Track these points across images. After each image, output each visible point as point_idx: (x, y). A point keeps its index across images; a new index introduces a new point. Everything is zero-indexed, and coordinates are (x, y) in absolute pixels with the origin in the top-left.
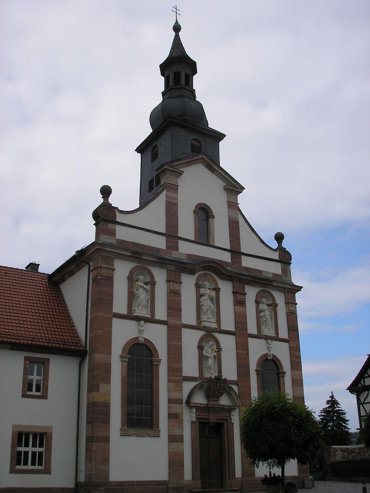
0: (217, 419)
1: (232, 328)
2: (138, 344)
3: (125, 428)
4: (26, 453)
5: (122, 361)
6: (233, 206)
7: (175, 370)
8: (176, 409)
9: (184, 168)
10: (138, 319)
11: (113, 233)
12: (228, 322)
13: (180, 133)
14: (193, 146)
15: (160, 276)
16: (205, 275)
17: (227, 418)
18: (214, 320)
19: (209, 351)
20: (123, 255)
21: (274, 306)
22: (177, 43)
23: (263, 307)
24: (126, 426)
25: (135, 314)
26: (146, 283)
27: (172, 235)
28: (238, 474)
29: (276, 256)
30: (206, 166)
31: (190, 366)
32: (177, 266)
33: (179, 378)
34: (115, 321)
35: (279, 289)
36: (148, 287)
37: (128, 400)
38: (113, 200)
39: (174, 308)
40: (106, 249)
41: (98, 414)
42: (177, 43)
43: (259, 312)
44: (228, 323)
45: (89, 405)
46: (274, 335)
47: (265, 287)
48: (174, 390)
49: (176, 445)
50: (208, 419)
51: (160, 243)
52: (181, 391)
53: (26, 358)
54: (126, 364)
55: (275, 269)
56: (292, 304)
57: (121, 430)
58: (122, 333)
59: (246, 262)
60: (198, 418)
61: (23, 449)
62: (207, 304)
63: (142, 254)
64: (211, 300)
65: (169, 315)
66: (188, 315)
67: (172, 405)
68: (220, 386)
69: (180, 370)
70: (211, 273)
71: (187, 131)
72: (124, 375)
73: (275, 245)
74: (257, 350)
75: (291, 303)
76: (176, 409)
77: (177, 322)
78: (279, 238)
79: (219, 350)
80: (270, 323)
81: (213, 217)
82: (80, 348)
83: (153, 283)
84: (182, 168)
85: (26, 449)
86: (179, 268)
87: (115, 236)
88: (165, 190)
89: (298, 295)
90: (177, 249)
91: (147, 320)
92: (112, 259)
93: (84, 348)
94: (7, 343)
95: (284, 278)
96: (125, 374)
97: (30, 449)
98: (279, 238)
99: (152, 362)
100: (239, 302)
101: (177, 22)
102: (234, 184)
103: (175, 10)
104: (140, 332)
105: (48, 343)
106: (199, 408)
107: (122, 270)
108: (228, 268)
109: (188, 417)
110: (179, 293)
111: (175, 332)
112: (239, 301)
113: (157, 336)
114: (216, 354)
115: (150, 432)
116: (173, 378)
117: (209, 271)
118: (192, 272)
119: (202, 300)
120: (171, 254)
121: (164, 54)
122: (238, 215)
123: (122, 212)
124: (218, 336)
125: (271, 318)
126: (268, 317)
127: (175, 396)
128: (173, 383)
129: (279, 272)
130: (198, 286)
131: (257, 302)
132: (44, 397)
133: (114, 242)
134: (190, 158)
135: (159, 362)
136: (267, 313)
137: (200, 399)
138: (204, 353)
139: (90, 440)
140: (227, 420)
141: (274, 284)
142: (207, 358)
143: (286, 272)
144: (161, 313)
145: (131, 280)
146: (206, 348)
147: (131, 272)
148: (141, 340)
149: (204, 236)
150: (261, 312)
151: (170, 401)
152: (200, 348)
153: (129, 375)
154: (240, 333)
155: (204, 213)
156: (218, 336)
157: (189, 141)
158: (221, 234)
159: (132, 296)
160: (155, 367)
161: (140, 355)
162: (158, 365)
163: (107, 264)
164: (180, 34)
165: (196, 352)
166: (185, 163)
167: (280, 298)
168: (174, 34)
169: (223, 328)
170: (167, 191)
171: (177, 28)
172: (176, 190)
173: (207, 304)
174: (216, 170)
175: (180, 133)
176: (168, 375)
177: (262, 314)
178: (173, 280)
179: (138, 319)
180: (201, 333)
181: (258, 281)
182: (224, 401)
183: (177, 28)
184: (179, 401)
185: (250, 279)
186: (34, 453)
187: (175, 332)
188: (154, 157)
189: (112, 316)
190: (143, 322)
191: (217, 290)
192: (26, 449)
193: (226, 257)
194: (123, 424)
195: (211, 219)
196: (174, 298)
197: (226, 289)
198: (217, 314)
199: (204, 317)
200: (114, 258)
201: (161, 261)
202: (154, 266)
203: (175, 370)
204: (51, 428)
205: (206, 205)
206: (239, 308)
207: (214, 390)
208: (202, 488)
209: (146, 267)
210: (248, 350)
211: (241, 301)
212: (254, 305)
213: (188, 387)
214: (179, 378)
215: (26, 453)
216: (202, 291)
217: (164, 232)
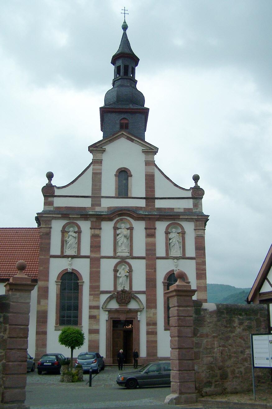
0: (126, 318)
2: (68, 273)
3: (58, 326)
5: (57, 285)
6: (150, 163)
7: (95, 290)
8: (95, 312)
9: (106, 146)
10: (68, 257)
12: (140, 249)
13: (125, 113)
16: (121, 220)
17: (135, 317)
20: (56, 217)
22: (125, 41)
24: (59, 324)
25: (66, 254)
27: (96, 197)
28: (143, 353)
30: (127, 139)
32: (96, 217)
33: (97, 292)
34: (52, 260)
38: (54, 182)
39: (96, 246)
40: (44, 216)
42: (125, 41)
43: (168, 239)
47: (174, 220)
48: (93, 300)
49: (93, 335)
50: (120, 318)
51: (87, 203)
52: (99, 301)
54: (60, 286)
55: (189, 204)
56: (200, 230)
57: (55, 327)
58: (57, 267)
59: (159, 204)
60: (111, 318)
63: (69, 215)
64: (125, 236)
65: (91, 251)
66: (107, 248)
67: (91, 310)
68: (125, 296)
69: (98, 287)
70: (129, 218)
71: (117, 114)
72: (58, 293)
74: (163, 269)
76: (95, 312)
79: (131, 271)
81: (131, 176)
83: (79, 232)
84: (104, 146)
86: (97, 219)
88: (92, 165)
90: (99, 205)
92: (50, 221)
96: (59, 293)
101: (125, 22)
102: (150, 146)
103: (123, 12)
104: (71, 265)
105: (35, 277)
106: (110, 311)
109: (104, 317)
110: (99, 236)
111: (95, 263)
112: (151, 234)
113: (82, 267)
114: (127, 274)
117: (125, 216)
118: (110, 219)
119: (118, 237)
120: (95, 209)
122: (154, 169)
123: (59, 188)
127: (94, 304)
128: (93, 296)
129: (191, 206)
134: (111, 137)
135: (83, 283)
137: (114, 305)
138: (118, 275)
140: (135, 318)
141: (181, 217)
144: (86, 250)
145: (64, 232)
147: (64, 227)
149: (123, 191)
151: (91, 307)
152: (116, 271)
155: (123, 174)
157: (118, 122)
158: (138, 187)
159: (63, 242)
161: (70, 280)
162: (82, 285)
165: (112, 274)
166: (108, 141)
168: (122, 31)
169: (135, 255)
170: (93, 165)
171: (125, 27)
173: (121, 240)
178: (96, 227)
179: (68, 257)
180: (116, 261)
181: (166, 217)
182: (133, 305)
183: (125, 27)
184: (97, 307)
185: (158, 217)
187: (95, 263)
189: (49, 257)
190: (70, 258)
191: (131, 229)
193: (142, 203)
194: (56, 324)
195: (129, 178)
198: (130, 246)
199: (119, 250)
200: (51, 220)
203: (95, 290)
205: (126, 168)
206: (150, 240)
207: (121, 299)
208: (113, 363)
209: (74, 222)
210: (155, 269)
211: (150, 234)
212: (164, 235)
213: (104, 297)
214: (97, 292)
216: (118, 232)
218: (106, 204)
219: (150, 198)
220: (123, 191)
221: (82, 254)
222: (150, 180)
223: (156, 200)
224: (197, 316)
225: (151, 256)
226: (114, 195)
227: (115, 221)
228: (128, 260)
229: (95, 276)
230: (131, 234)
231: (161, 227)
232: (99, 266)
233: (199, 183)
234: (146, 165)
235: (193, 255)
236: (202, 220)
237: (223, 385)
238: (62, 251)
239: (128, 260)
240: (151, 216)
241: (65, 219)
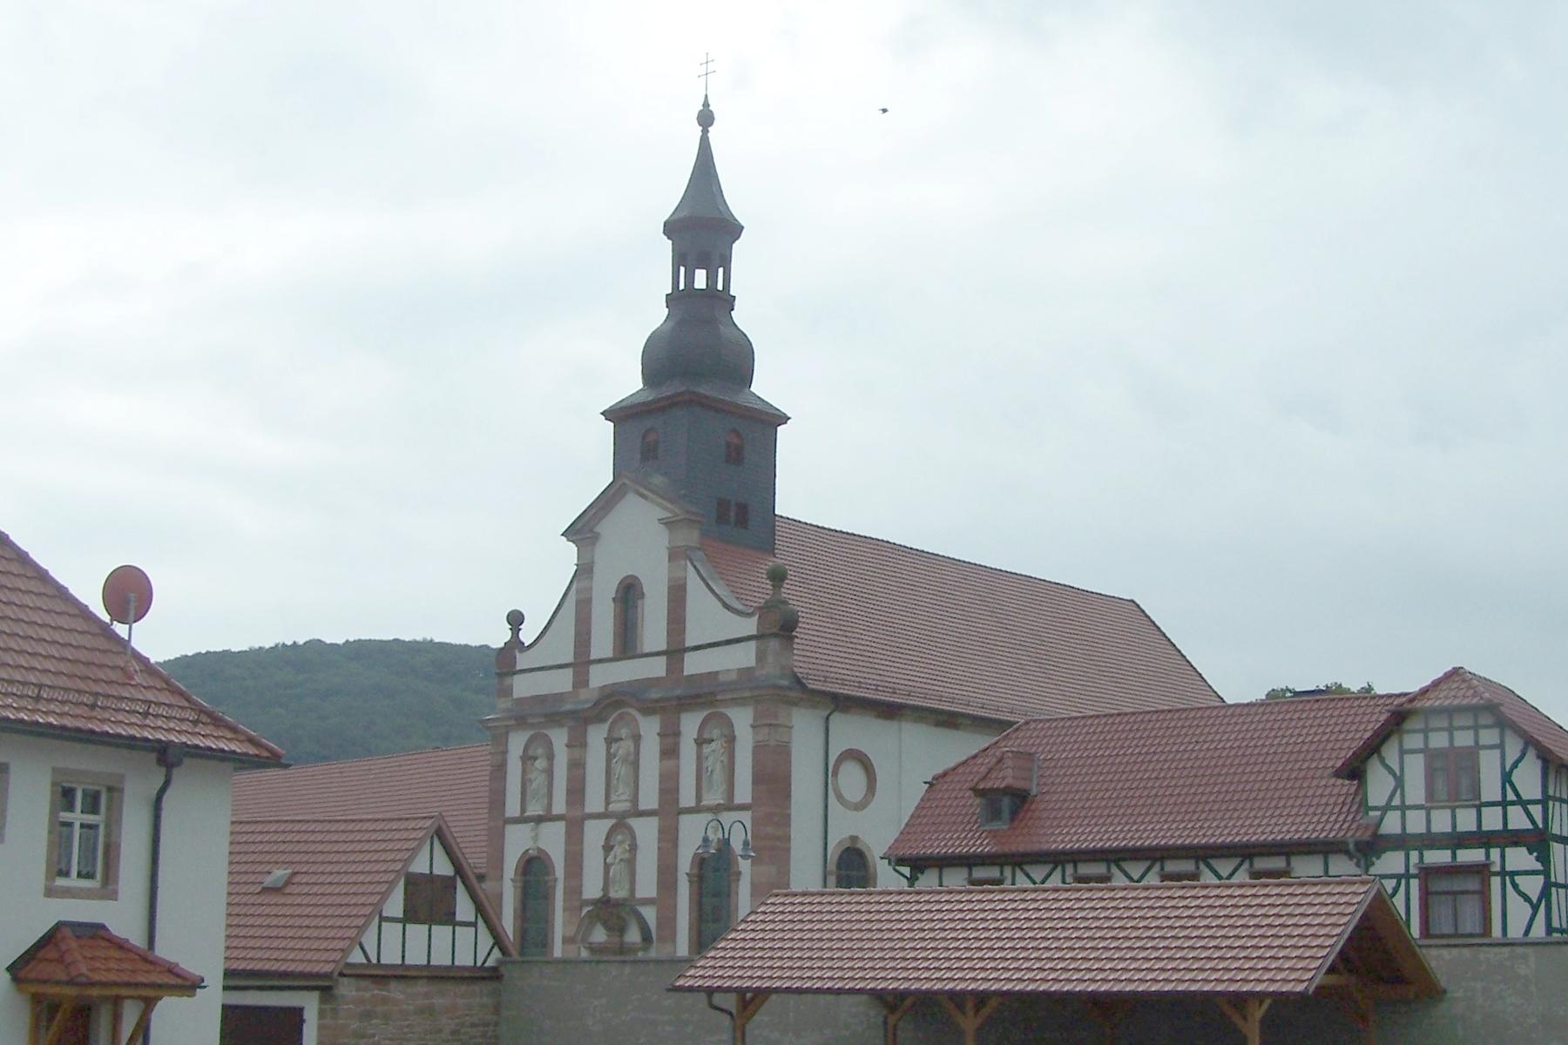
7: (574, 890)
10: (710, 809)
13: (696, 418)
16: (621, 717)
27: (582, 663)
39: (576, 792)
44: (649, 798)
58: (518, 841)
59: (694, 664)
62: (621, 770)
66: (594, 801)
74: (692, 834)
79: (633, 848)
80: (719, 776)
100: (670, 751)
104: (536, 838)
113: (553, 840)
118: (601, 719)
121: (669, 194)
130: (610, 741)
144: (559, 807)
155: (629, 593)
158: (654, 633)
164: (713, 132)
168: (697, 131)
171: (706, 119)
175: (696, 418)
178: (578, 743)
183: (706, 119)
203: (574, 890)
206: (669, 763)
218: (601, 677)
219: (675, 652)
220: (626, 646)
221: (738, 800)
224: (1351, 846)
226: (610, 654)
231: (690, 724)
233: (787, 591)
235: (748, 800)
238: (523, 810)
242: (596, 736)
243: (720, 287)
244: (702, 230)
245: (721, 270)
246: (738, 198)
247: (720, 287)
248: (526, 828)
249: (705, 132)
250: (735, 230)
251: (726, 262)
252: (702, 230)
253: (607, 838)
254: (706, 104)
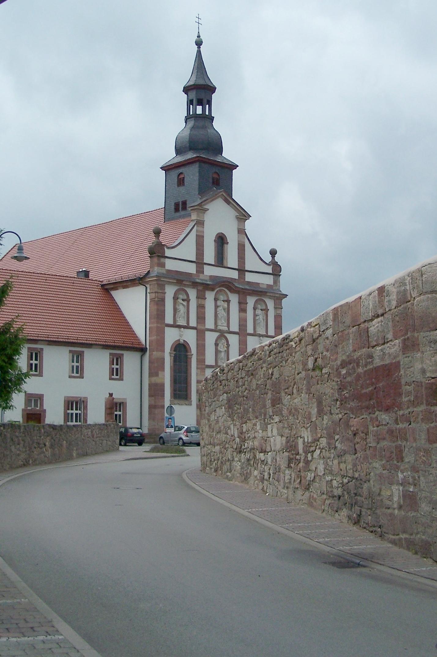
1: (237, 330)
2: (179, 344)
4: (72, 414)
6: (242, 231)
7: (201, 361)
10: (179, 327)
11: (163, 265)
13: (202, 167)
14: (213, 179)
15: (192, 293)
16: (221, 291)
18: (225, 324)
19: (222, 348)
21: (266, 310)
22: (199, 65)
23: (258, 312)
26: (183, 300)
27: (200, 263)
29: (269, 269)
31: (210, 359)
35: (270, 297)
36: (185, 303)
37: (175, 381)
39: (201, 318)
41: (156, 391)
43: (255, 315)
44: (234, 327)
45: (150, 385)
46: (265, 333)
47: (261, 296)
51: (191, 269)
53: (111, 354)
55: (268, 280)
58: (171, 336)
59: (249, 277)
61: (70, 411)
62: (222, 313)
63: (183, 281)
66: (210, 323)
69: (204, 361)
73: (268, 258)
75: (278, 306)
77: (203, 328)
78: (273, 253)
79: (228, 345)
80: (263, 324)
82: (141, 346)
83: (188, 300)
85: (72, 412)
86: (203, 287)
87: (165, 267)
89: (283, 300)
91: (185, 327)
93: (144, 346)
94: (100, 345)
95: (274, 288)
97: (74, 412)
98: (273, 253)
99: (186, 356)
100: (243, 310)
102: (244, 213)
107: (170, 291)
108: (237, 285)
111: (201, 334)
113: (190, 337)
115: (187, 402)
116: (200, 366)
121: (186, 75)
124: (228, 336)
125: (263, 320)
126: (261, 320)
130: (216, 300)
131: (255, 309)
132: (121, 379)
133: (164, 272)
136: (261, 317)
139: (151, 407)
142: (221, 352)
143: (276, 282)
144: (193, 322)
145: (175, 298)
146: (220, 345)
147: (175, 294)
148: (182, 341)
149: (220, 261)
150: (257, 316)
152: (216, 345)
153: (174, 365)
154: (242, 333)
155: (221, 240)
156: (228, 336)
158: (232, 259)
160: (188, 359)
161: (181, 349)
163: (161, 290)
165: (214, 347)
167: (270, 304)
171: (199, 43)
172: (203, 224)
173: (222, 313)
174: (230, 202)
175: (202, 167)
176: (197, 365)
177: (257, 318)
178: (201, 297)
179: (179, 327)
180: (217, 334)
183: (199, 43)
186: (76, 414)
187: (201, 334)
188: (181, 182)
192: (72, 412)
193: (235, 275)
196: (201, 308)
197: (234, 299)
199: (219, 323)
201: (195, 284)
202: (189, 287)
204: (125, 399)
206: (243, 314)
215: (72, 414)
217: (195, 260)
220: (220, 261)
222: (241, 248)
223: (246, 273)
225: (242, 333)
227: (216, 291)
228: (226, 335)
229: (201, 348)
230: (228, 305)
231: (251, 301)
232: (204, 340)
233: (161, 239)
234: (238, 233)
236: (279, 298)
237: (423, 384)
239: (226, 335)
240: (241, 289)
241: (177, 286)
242: (210, 296)
243: (207, 113)
244: (200, 92)
245: (207, 106)
246: (214, 78)
247: (207, 113)
248: (175, 330)
249: (199, 48)
250: (213, 89)
251: (209, 103)
252: (200, 92)
253: (216, 341)
254: (199, 36)
